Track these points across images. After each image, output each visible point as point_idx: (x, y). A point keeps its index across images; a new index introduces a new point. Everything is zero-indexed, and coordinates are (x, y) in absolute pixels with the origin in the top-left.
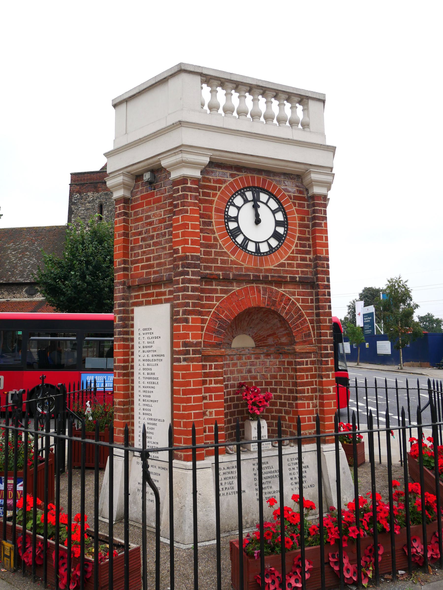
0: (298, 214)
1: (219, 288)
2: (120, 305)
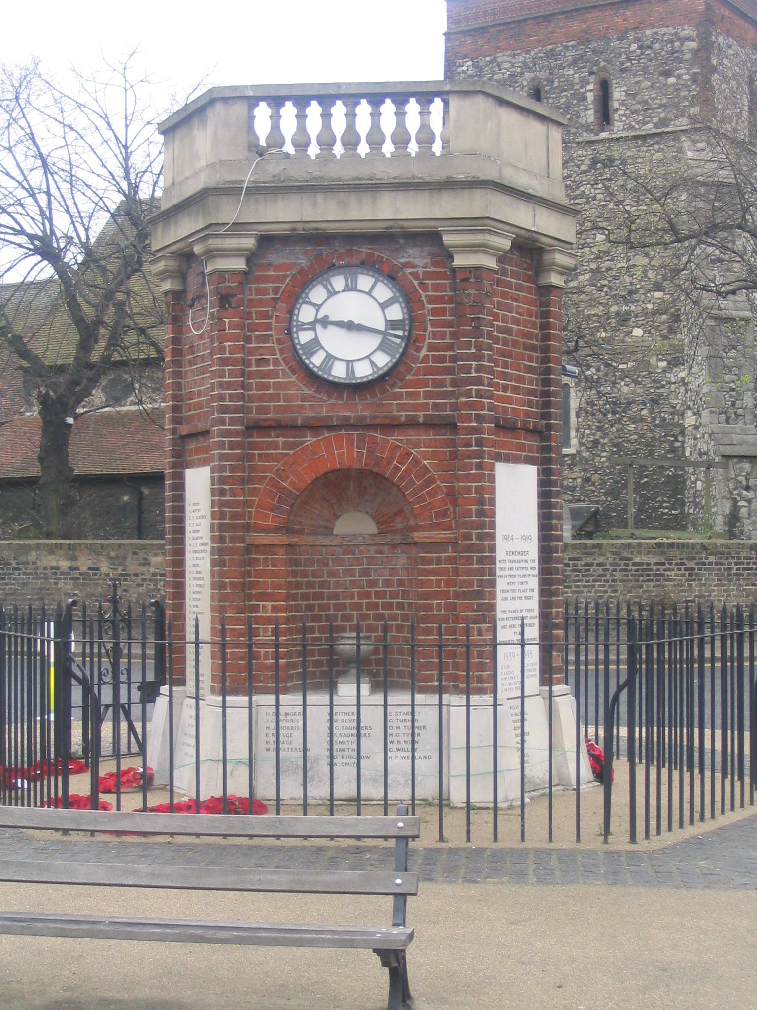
1: (281, 440)
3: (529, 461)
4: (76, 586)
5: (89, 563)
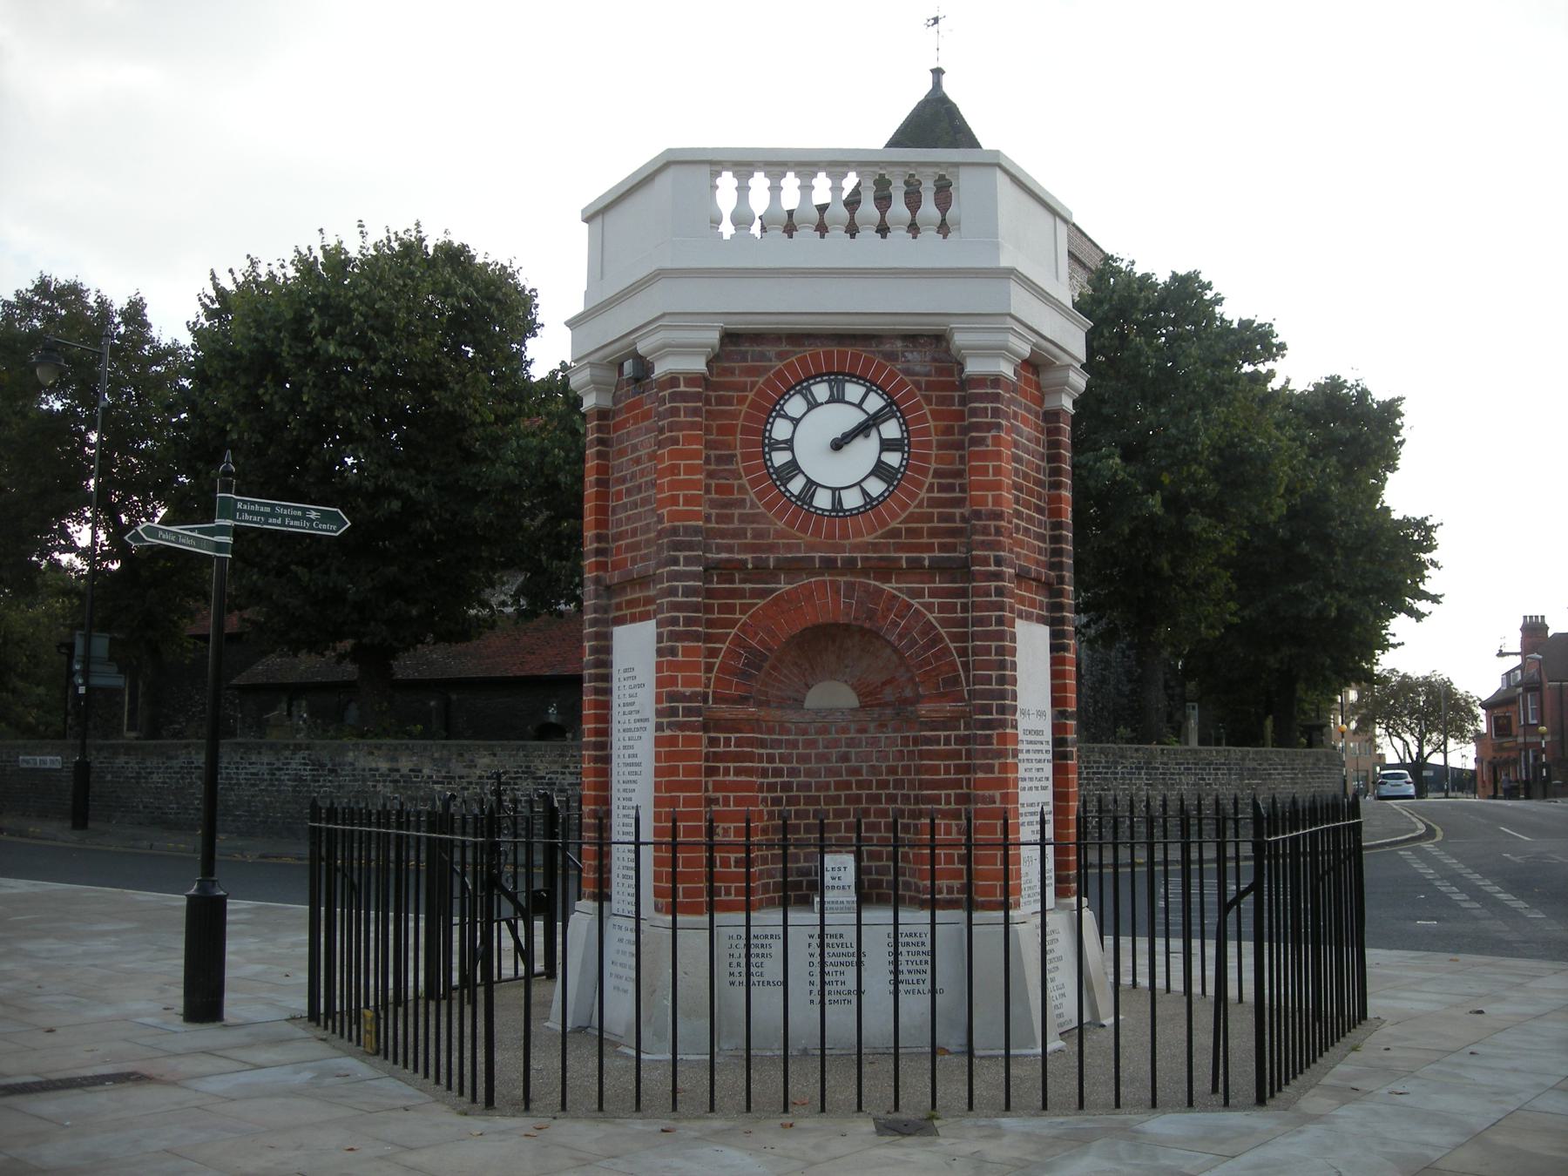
0: (934, 419)
2: (594, 623)
3: (1041, 620)
4: (396, 789)
5: (411, 766)
